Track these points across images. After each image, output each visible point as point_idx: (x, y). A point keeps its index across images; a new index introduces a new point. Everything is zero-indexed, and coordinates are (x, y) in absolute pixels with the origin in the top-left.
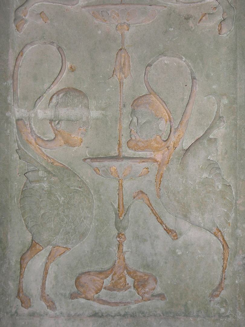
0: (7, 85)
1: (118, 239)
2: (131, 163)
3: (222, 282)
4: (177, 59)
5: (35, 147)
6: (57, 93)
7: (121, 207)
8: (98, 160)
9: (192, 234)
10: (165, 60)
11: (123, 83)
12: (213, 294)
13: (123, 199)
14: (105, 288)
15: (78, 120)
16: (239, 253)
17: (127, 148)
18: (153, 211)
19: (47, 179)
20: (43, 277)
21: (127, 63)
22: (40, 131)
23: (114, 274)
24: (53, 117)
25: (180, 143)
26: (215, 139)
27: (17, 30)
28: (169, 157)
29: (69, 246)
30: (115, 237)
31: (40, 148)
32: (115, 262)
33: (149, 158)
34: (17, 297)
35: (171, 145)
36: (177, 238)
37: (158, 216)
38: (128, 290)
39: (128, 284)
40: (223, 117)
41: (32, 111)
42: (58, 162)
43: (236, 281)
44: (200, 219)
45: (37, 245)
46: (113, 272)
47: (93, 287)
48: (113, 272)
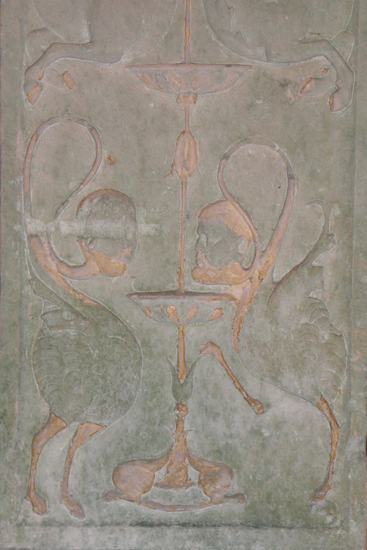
0: (14, 184)
1: (177, 412)
2: (197, 301)
3: (328, 477)
4: (268, 149)
5: (57, 277)
6: (90, 197)
7: (181, 364)
8: (150, 296)
9: (285, 406)
10: (250, 149)
11: (186, 183)
12: (315, 495)
13: (184, 353)
14: (156, 485)
15: (120, 238)
16: (353, 434)
17: (191, 279)
18: (229, 371)
19: (75, 323)
20: (65, 468)
21: (192, 153)
22: (63, 253)
23: (170, 465)
24: (82, 232)
25: (268, 273)
26: (321, 267)
27: (28, 101)
28: (251, 293)
29: (105, 422)
30: (173, 409)
31: (64, 277)
32: (172, 446)
33: (224, 295)
34: (25, 498)
35: (256, 275)
36: (263, 412)
37: (236, 379)
38: (191, 488)
39: (190, 479)
40: (332, 235)
41: (51, 223)
42: (90, 299)
43: (348, 475)
44: (296, 383)
45: (59, 420)
46: (169, 462)
47: (139, 482)
48: (169, 462)
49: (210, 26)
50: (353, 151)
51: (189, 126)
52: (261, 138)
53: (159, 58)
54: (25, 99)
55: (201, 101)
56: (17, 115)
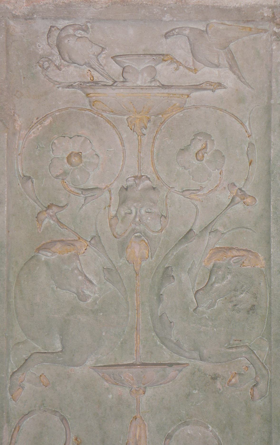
10: (189, 430)
49: (156, 333)
50: (271, 433)
51: (139, 412)
52: (197, 421)
53: (116, 359)
54: (9, 398)
55: (150, 391)
56: (4, 412)
